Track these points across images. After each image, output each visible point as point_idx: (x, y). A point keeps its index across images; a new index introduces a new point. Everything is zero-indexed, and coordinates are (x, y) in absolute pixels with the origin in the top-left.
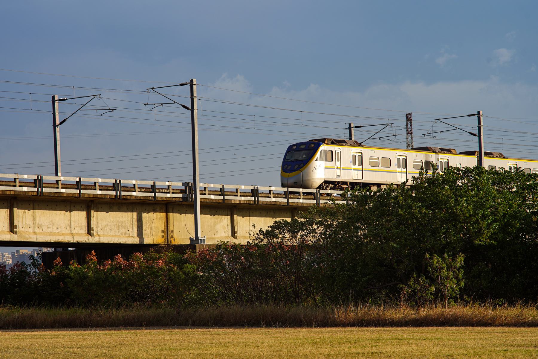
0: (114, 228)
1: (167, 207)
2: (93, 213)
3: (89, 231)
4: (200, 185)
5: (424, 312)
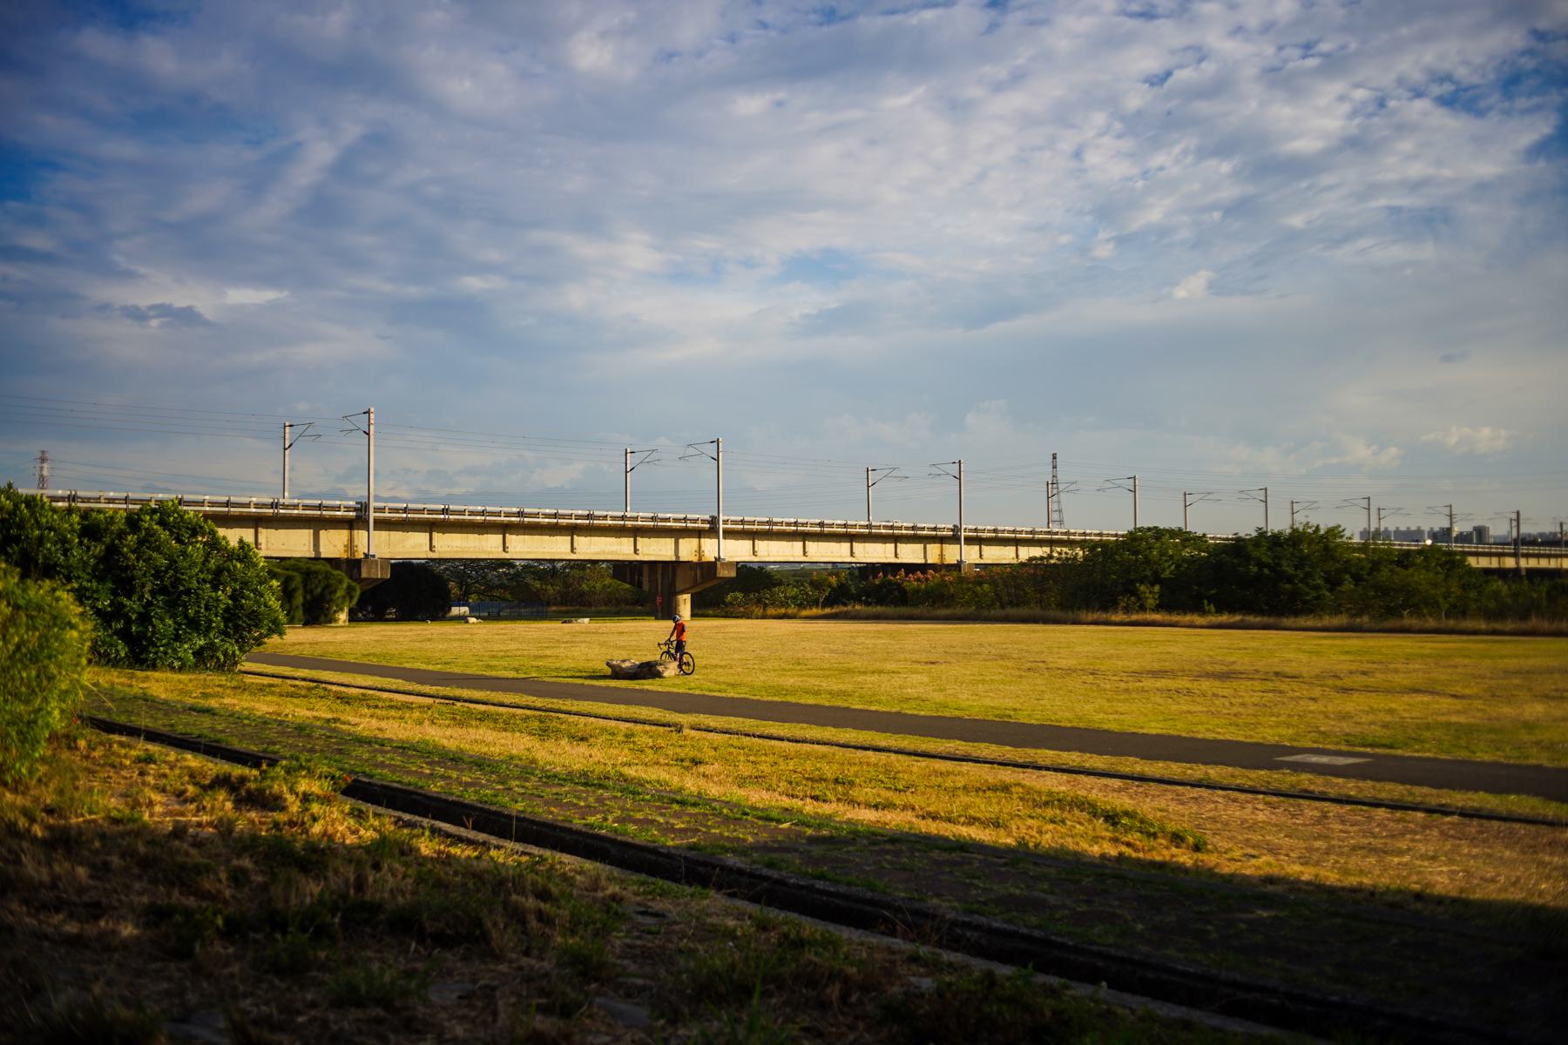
0: (910, 554)
1: (942, 540)
2: (435, 535)
3: (505, 549)
4: (722, 518)
5: (1135, 617)
